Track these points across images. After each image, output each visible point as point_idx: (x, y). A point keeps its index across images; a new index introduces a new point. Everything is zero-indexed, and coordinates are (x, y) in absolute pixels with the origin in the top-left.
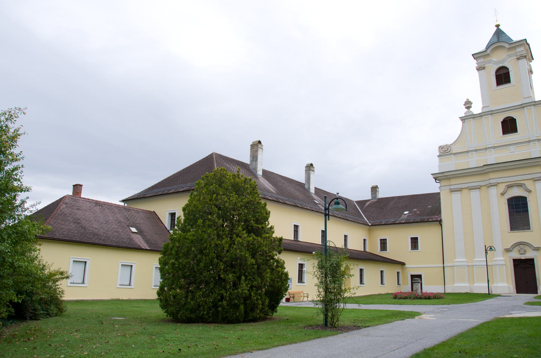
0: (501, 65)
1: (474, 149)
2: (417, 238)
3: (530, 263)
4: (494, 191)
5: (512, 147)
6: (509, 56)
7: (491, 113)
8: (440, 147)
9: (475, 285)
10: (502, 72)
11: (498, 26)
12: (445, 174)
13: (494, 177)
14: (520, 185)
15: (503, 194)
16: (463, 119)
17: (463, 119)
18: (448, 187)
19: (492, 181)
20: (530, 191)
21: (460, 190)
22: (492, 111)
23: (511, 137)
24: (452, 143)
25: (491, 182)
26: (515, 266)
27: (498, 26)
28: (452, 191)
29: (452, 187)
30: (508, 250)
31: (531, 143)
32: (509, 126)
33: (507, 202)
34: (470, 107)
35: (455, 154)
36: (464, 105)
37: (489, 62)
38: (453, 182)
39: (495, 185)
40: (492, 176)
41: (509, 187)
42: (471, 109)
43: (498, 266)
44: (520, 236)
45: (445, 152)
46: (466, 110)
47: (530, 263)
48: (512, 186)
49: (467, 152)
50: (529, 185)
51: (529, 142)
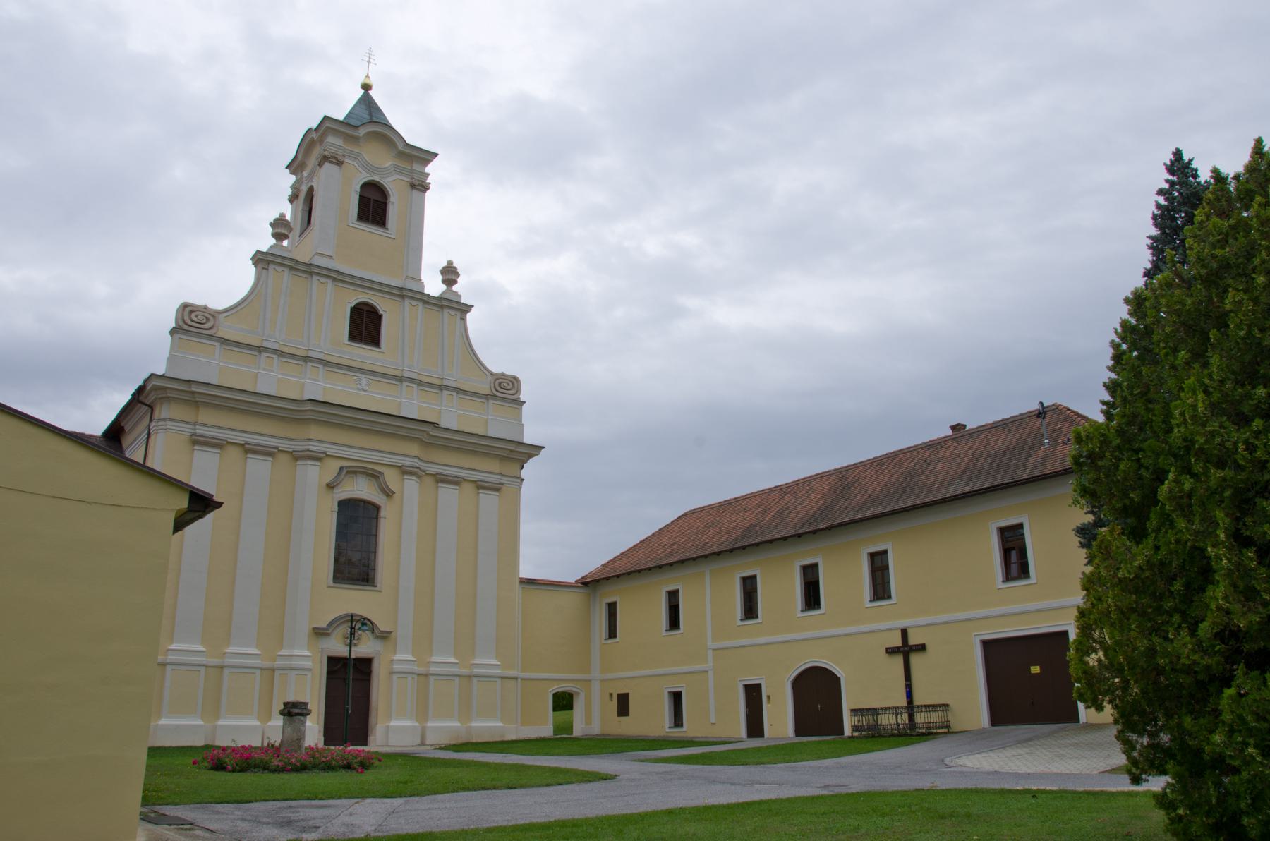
0: (376, 178)
1: (276, 347)
2: (615, 603)
3: (364, 667)
4: (313, 475)
5: (364, 379)
6: (398, 170)
7: (292, 264)
8: (185, 306)
9: (221, 722)
10: (373, 195)
11: (367, 87)
12: (194, 388)
13: (317, 437)
14: (374, 476)
15: (330, 486)
16: (261, 260)
17: (261, 260)
18: (188, 429)
19: (314, 446)
20: (388, 493)
21: (218, 445)
22: (296, 261)
23: (361, 353)
24: (221, 307)
25: (311, 448)
26: (331, 673)
27: (367, 87)
28: (195, 443)
29: (200, 431)
30: (320, 633)
31: (405, 384)
32: (365, 325)
33: (336, 509)
34: (455, 282)
35: (224, 341)
36: (271, 225)
37: (356, 157)
38: (206, 416)
39: (317, 458)
40: (315, 432)
41: (353, 472)
42: (455, 288)
43: (475, 680)
44: (354, 600)
45: (193, 323)
46: (273, 241)
47: (364, 667)
48: (355, 472)
49: (259, 349)
50: (391, 478)
51: (401, 379)
